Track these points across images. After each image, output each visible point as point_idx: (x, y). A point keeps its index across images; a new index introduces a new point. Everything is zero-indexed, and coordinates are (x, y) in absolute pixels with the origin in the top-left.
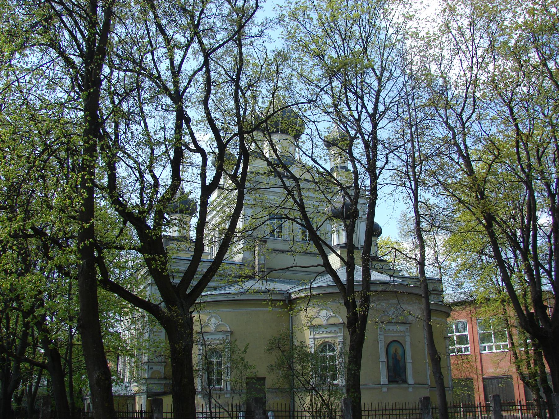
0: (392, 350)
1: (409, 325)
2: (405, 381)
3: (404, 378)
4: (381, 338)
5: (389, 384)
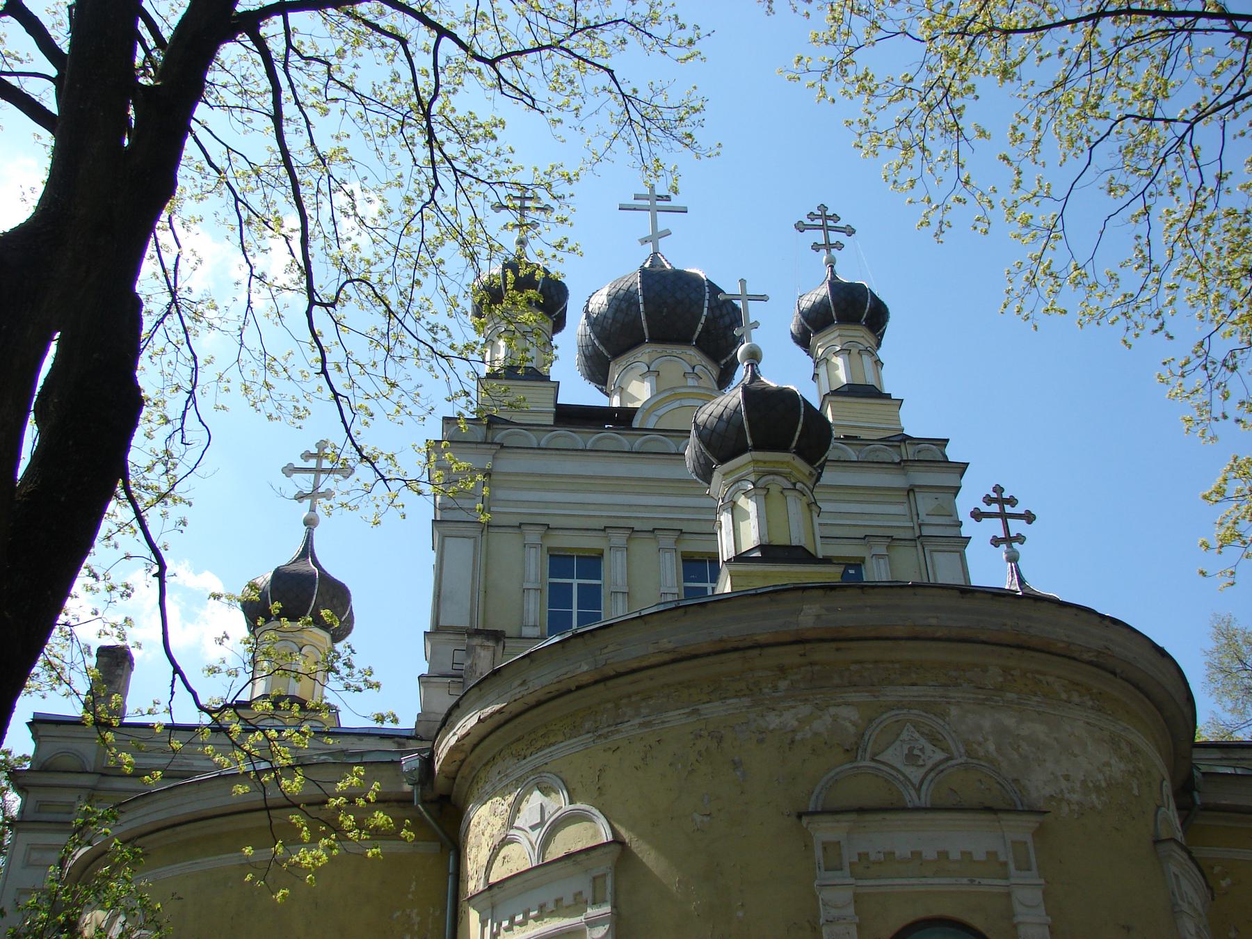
1: (1032, 821)
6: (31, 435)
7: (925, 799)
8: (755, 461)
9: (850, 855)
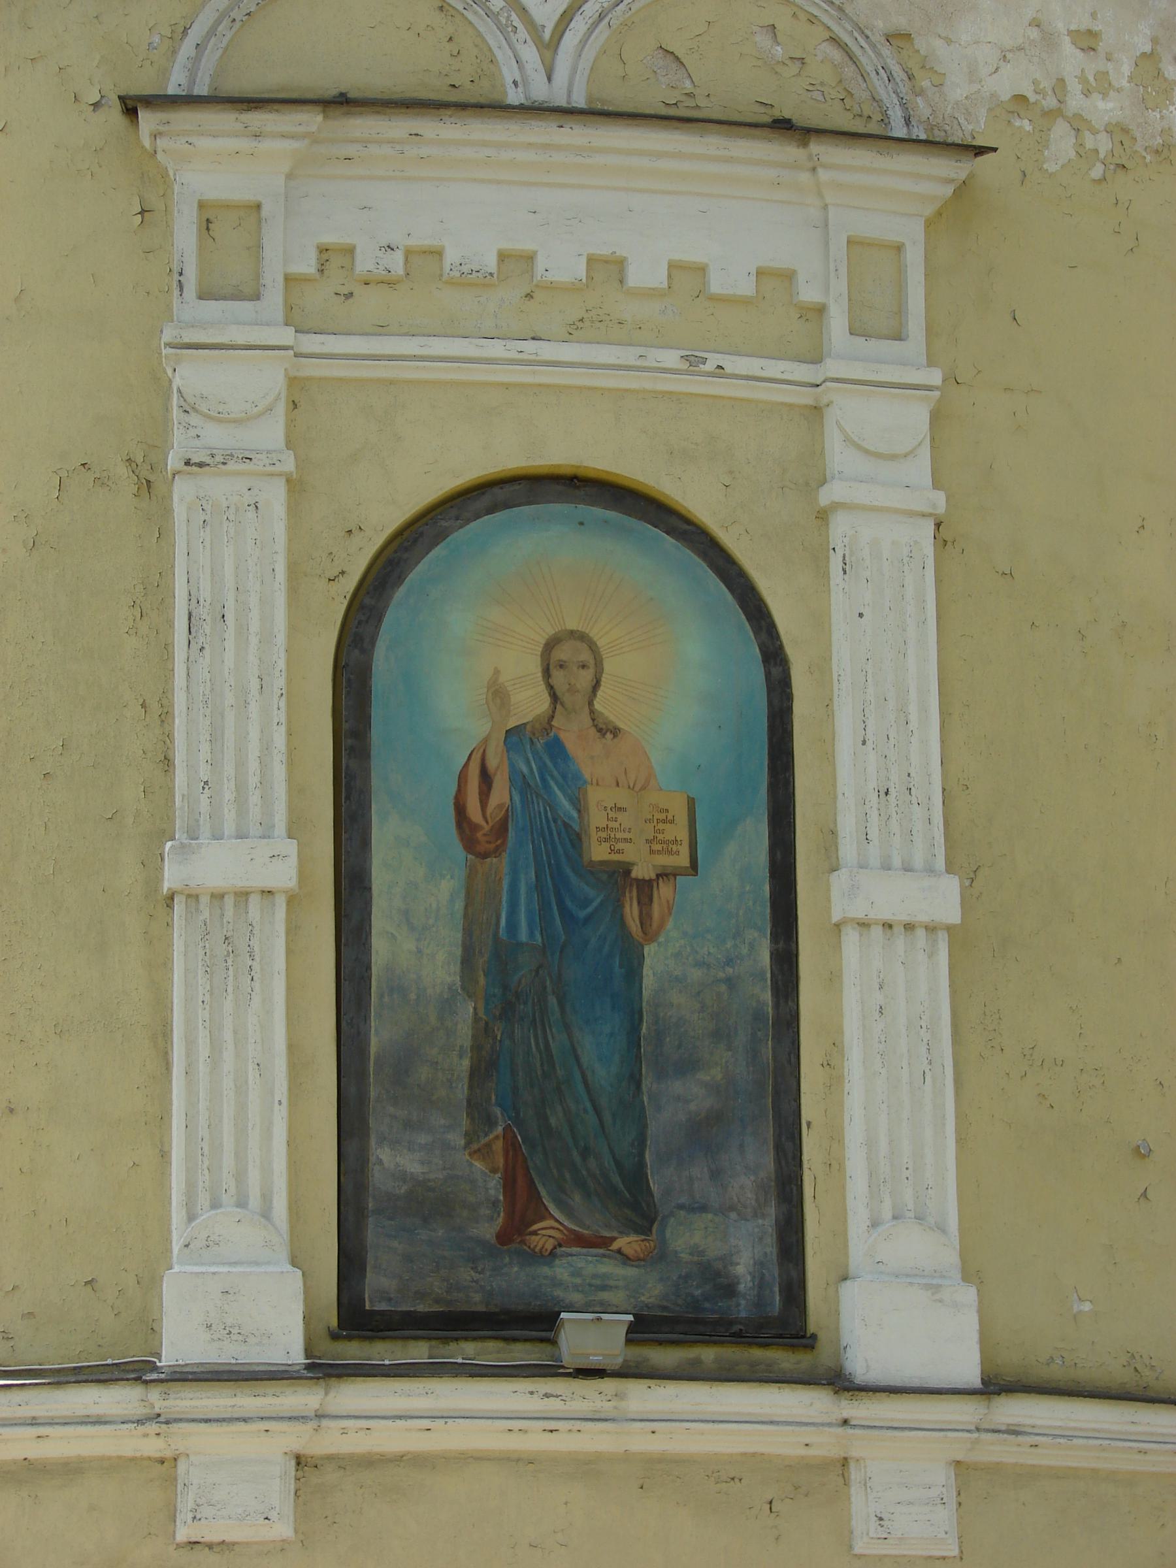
0: (472, 664)
1: (936, 175)
2: (756, 1322)
3: (746, 1252)
4: (232, 388)
5: (321, 1369)
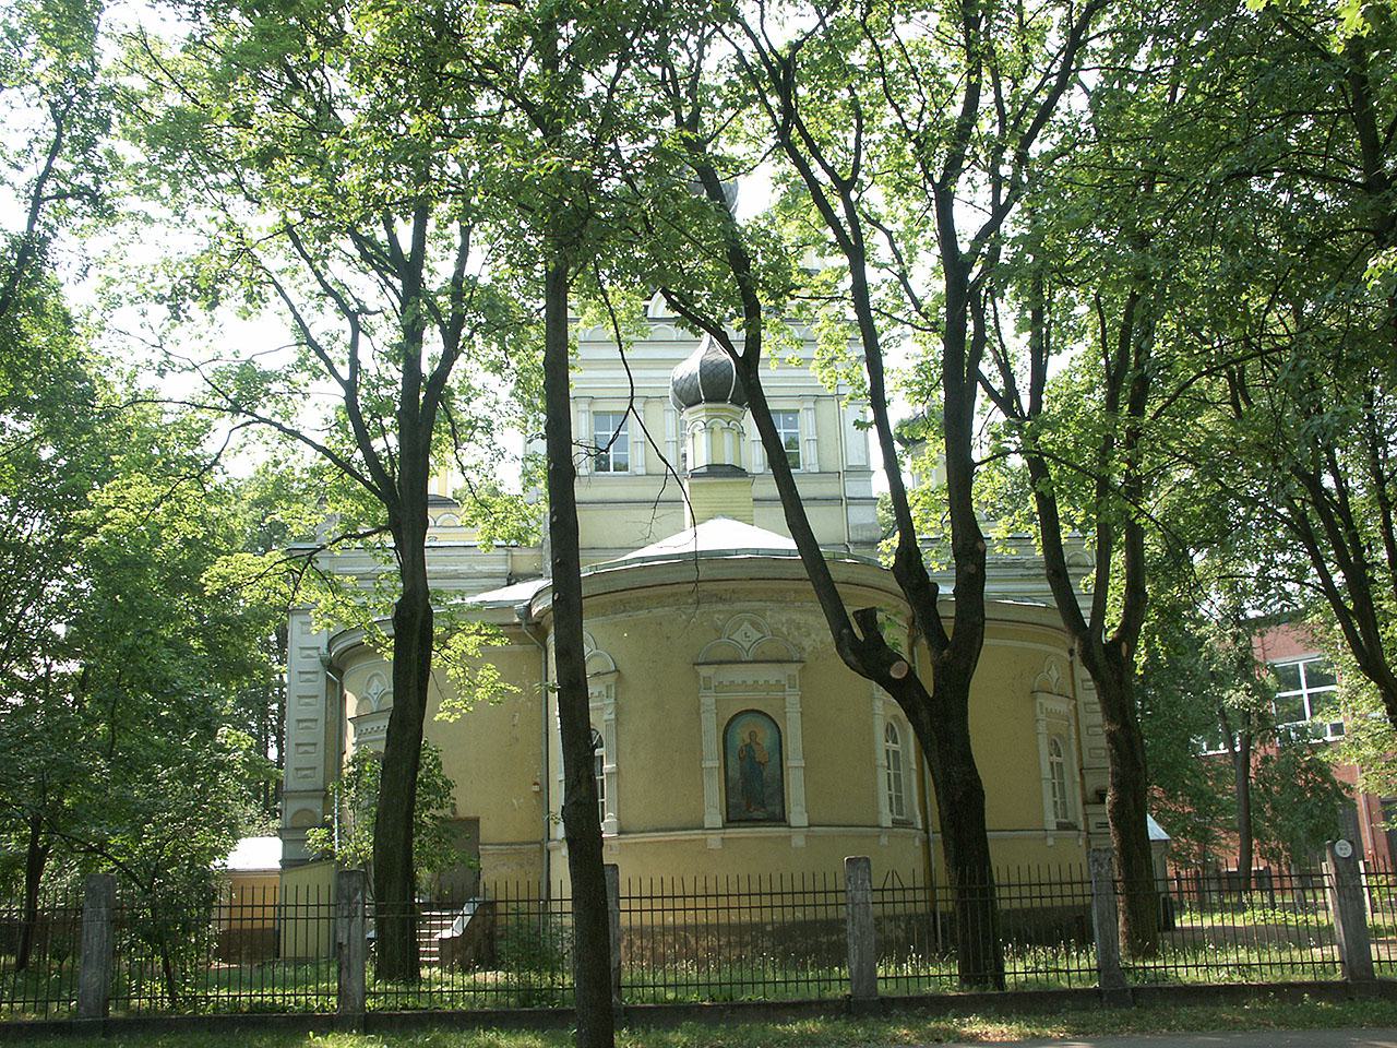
0: (740, 736)
1: (800, 666)
2: (780, 819)
3: (778, 810)
4: (708, 701)
5: (724, 827)
6: (422, 394)
7: (750, 658)
8: (707, 409)
9: (714, 683)
